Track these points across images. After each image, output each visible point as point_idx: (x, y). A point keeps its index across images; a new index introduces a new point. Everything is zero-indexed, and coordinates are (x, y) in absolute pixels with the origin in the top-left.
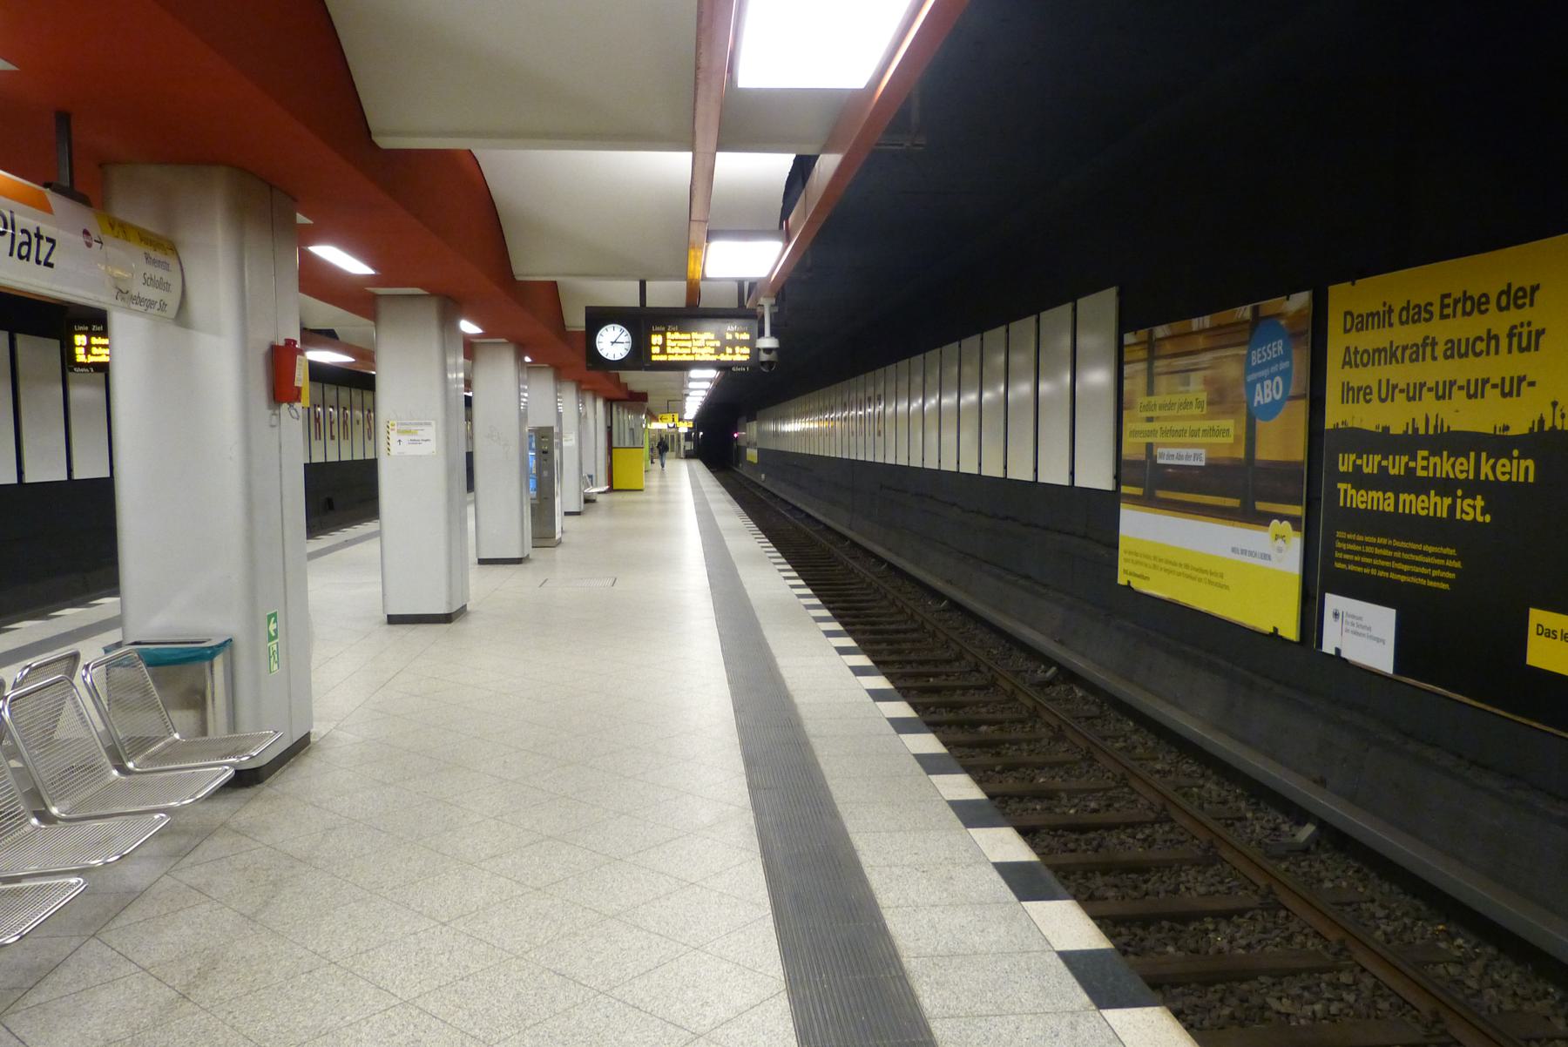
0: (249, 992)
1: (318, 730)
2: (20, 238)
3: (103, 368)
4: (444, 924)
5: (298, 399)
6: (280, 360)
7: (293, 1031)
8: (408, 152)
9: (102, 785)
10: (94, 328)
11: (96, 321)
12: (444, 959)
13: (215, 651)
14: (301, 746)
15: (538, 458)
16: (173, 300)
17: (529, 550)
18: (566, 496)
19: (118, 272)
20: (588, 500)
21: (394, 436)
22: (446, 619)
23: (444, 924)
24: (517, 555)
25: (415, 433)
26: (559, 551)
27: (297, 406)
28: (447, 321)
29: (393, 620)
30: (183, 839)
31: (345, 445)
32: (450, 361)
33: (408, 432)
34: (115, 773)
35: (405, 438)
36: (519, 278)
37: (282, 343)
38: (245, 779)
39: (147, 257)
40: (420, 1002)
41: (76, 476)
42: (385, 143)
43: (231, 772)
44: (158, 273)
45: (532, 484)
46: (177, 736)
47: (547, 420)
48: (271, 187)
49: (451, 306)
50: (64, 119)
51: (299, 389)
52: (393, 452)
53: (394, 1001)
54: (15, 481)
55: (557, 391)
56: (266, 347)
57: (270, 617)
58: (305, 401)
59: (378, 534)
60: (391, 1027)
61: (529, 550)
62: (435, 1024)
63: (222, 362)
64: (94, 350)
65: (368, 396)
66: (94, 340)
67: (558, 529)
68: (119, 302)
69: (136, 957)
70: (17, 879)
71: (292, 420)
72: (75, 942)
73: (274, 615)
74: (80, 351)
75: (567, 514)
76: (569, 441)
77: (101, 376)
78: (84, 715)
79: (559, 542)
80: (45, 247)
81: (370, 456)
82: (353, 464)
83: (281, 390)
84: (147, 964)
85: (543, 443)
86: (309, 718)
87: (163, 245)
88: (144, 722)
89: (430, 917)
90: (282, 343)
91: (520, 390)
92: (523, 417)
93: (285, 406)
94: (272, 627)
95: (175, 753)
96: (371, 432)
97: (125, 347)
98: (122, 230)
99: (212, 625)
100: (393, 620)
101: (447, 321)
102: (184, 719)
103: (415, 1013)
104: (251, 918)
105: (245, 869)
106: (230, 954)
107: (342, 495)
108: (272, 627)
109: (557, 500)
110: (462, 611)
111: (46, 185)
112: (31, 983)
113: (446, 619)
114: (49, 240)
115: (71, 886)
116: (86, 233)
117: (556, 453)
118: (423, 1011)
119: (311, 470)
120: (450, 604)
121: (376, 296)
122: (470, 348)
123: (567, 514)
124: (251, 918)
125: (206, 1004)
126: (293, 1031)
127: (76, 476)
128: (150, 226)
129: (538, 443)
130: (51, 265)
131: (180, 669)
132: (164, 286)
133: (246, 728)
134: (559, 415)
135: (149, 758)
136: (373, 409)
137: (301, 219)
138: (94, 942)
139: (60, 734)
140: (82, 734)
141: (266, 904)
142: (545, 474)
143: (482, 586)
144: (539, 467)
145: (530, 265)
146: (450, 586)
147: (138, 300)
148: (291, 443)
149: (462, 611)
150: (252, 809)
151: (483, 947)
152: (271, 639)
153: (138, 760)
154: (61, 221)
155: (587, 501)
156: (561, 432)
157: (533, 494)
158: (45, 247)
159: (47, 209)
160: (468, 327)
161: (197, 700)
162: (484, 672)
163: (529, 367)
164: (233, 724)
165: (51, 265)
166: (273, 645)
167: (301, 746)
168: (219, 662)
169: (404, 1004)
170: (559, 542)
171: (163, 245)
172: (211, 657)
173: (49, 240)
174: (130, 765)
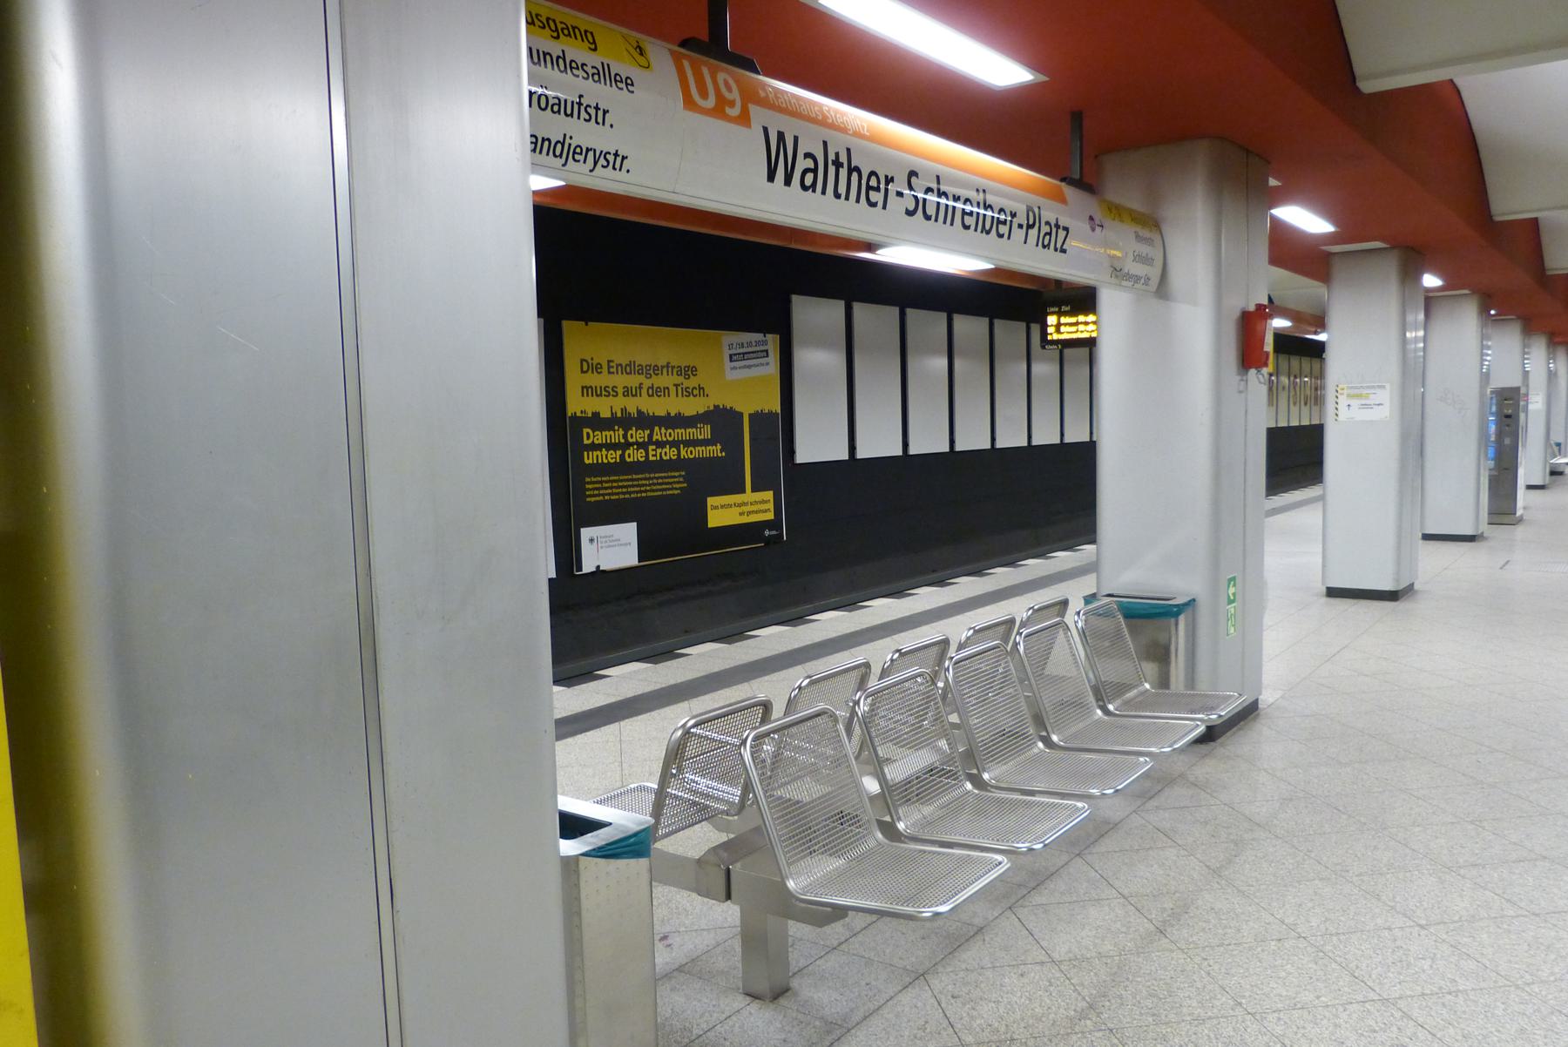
0: (1221, 945)
1: (1267, 698)
2: (1045, 229)
3: (1090, 343)
4: (1422, 927)
5: (1266, 365)
6: (1250, 323)
7: (1267, 995)
8: (1387, 92)
9: (1088, 722)
10: (1064, 308)
11: (1082, 300)
12: (1426, 964)
13: (1180, 609)
14: (1250, 712)
15: (1499, 423)
16: (1154, 272)
17: (1484, 527)
18: (1530, 468)
19: (1113, 252)
20: (1555, 473)
21: (1343, 401)
22: (1392, 596)
23: (1422, 927)
24: (1469, 532)
25: (1367, 398)
26: (1519, 531)
27: (1265, 371)
28: (1409, 273)
29: (1332, 593)
30: (1157, 783)
31: (1305, 410)
32: (1410, 318)
33: (1359, 396)
34: (1099, 712)
35: (1355, 403)
36: (1498, 219)
37: (1252, 308)
38: (1210, 735)
39: (1137, 236)
40: (1402, 1004)
41: (860, 455)
42: (1367, 86)
43: (1202, 729)
44: (1144, 249)
45: (1491, 452)
46: (1147, 686)
47: (1513, 381)
48: (1248, 151)
49: (1413, 258)
50: (1077, 117)
51: (1267, 354)
52: (1341, 418)
53: (1372, 995)
54: (946, 449)
55: (1525, 346)
56: (1237, 314)
57: (1230, 580)
58: (1270, 368)
59: (1322, 498)
60: (1372, 1023)
61: (1484, 527)
62: (1422, 1034)
63: (1197, 330)
64: (1063, 329)
65: (1316, 364)
66: (1064, 320)
67: (1520, 503)
68: (1114, 280)
69: (1117, 884)
70: (1032, 793)
71: (1257, 381)
72: (1065, 858)
73: (1234, 579)
74: (1051, 330)
75: (1530, 487)
76: (1536, 403)
77: (1087, 350)
78: (1069, 655)
79: (1520, 520)
80: (1062, 234)
81: (1076, 434)
82: (1300, 429)
83: (1249, 357)
84: (1126, 892)
85: (1506, 410)
86: (1258, 687)
87: (1149, 223)
88: (1113, 670)
89: (1405, 915)
90: (1252, 308)
91: (1483, 347)
92: (1485, 377)
93: (1253, 372)
94: (1232, 590)
95: (1144, 702)
96: (1317, 398)
97: (1112, 325)
98: (1117, 212)
99: (1179, 585)
100: (1332, 593)
101: (1409, 273)
102: (1150, 668)
103: (1398, 1015)
104: (1216, 872)
105: (1206, 823)
106: (1200, 902)
107: (1295, 458)
108: (1232, 590)
109: (1521, 472)
110: (1410, 589)
111: (1063, 180)
112: (1033, 884)
113: (1392, 596)
114: (1066, 229)
115: (1078, 809)
116: (1091, 218)
117: (1522, 416)
118: (1406, 1015)
119: (1274, 435)
120: (1397, 580)
121: (1330, 254)
122: (1430, 301)
123: (1530, 487)
124: (1216, 872)
125: (1182, 945)
126: (1267, 995)
127: (860, 455)
128: (1135, 203)
129: (1500, 406)
130: (1064, 251)
131: (1149, 623)
132: (1146, 260)
133: (1203, 686)
134: (1526, 374)
135: (1127, 703)
136: (1321, 375)
137: (1273, 182)
138: (1078, 860)
139: (1051, 669)
140: (1074, 673)
141: (1230, 862)
142: (1507, 441)
143: (1434, 563)
144: (1500, 434)
145: (1508, 204)
146: (1398, 562)
147: (1128, 277)
148: (1258, 408)
149: (1410, 589)
150: (1208, 767)
151: (1472, 965)
152: (1230, 602)
153: (1119, 702)
154: (1072, 210)
155: (1553, 473)
156: (1527, 395)
157: (1491, 464)
158: (1062, 234)
159: (1063, 201)
160: (1431, 281)
161: (1160, 654)
162: (1432, 656)
163: (1496, 321)
164: (1191, 681)
165: (1064, 251)
166: (1231, 608)
167: (1250, 712)
168: (1182, 618)
169: (1384, 1001)
170: (1520, 520)
171: (1149, 223)
172: (1177, 615)
173: (1066, 229)
174: (1111, 707)
